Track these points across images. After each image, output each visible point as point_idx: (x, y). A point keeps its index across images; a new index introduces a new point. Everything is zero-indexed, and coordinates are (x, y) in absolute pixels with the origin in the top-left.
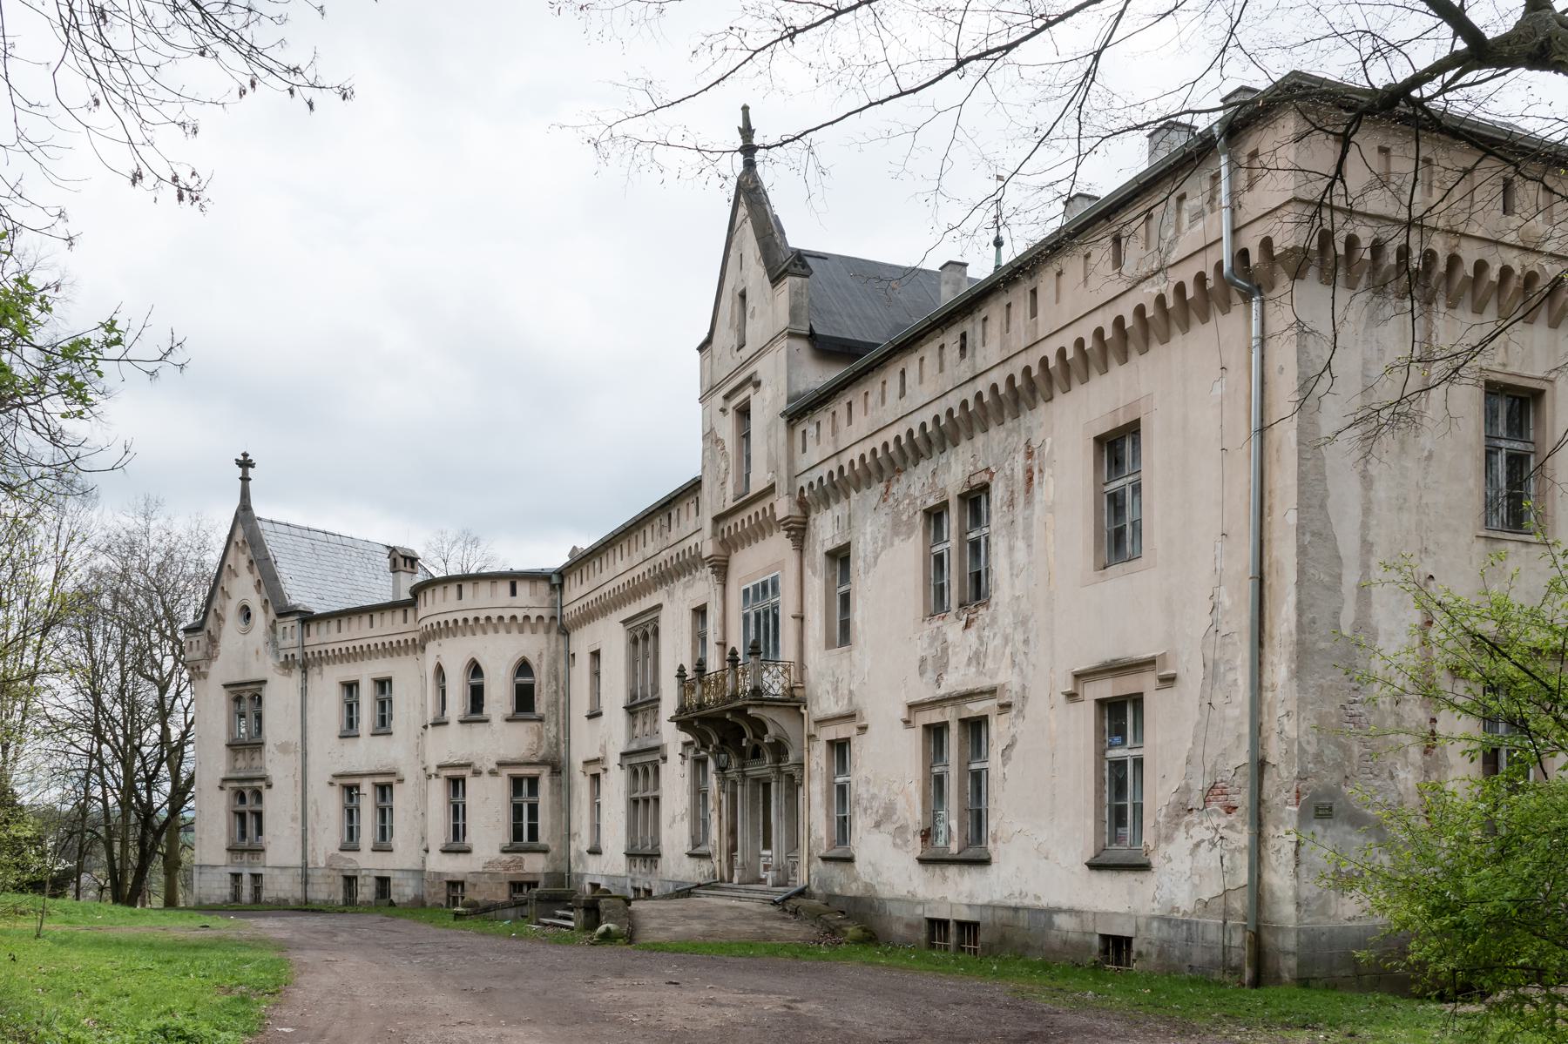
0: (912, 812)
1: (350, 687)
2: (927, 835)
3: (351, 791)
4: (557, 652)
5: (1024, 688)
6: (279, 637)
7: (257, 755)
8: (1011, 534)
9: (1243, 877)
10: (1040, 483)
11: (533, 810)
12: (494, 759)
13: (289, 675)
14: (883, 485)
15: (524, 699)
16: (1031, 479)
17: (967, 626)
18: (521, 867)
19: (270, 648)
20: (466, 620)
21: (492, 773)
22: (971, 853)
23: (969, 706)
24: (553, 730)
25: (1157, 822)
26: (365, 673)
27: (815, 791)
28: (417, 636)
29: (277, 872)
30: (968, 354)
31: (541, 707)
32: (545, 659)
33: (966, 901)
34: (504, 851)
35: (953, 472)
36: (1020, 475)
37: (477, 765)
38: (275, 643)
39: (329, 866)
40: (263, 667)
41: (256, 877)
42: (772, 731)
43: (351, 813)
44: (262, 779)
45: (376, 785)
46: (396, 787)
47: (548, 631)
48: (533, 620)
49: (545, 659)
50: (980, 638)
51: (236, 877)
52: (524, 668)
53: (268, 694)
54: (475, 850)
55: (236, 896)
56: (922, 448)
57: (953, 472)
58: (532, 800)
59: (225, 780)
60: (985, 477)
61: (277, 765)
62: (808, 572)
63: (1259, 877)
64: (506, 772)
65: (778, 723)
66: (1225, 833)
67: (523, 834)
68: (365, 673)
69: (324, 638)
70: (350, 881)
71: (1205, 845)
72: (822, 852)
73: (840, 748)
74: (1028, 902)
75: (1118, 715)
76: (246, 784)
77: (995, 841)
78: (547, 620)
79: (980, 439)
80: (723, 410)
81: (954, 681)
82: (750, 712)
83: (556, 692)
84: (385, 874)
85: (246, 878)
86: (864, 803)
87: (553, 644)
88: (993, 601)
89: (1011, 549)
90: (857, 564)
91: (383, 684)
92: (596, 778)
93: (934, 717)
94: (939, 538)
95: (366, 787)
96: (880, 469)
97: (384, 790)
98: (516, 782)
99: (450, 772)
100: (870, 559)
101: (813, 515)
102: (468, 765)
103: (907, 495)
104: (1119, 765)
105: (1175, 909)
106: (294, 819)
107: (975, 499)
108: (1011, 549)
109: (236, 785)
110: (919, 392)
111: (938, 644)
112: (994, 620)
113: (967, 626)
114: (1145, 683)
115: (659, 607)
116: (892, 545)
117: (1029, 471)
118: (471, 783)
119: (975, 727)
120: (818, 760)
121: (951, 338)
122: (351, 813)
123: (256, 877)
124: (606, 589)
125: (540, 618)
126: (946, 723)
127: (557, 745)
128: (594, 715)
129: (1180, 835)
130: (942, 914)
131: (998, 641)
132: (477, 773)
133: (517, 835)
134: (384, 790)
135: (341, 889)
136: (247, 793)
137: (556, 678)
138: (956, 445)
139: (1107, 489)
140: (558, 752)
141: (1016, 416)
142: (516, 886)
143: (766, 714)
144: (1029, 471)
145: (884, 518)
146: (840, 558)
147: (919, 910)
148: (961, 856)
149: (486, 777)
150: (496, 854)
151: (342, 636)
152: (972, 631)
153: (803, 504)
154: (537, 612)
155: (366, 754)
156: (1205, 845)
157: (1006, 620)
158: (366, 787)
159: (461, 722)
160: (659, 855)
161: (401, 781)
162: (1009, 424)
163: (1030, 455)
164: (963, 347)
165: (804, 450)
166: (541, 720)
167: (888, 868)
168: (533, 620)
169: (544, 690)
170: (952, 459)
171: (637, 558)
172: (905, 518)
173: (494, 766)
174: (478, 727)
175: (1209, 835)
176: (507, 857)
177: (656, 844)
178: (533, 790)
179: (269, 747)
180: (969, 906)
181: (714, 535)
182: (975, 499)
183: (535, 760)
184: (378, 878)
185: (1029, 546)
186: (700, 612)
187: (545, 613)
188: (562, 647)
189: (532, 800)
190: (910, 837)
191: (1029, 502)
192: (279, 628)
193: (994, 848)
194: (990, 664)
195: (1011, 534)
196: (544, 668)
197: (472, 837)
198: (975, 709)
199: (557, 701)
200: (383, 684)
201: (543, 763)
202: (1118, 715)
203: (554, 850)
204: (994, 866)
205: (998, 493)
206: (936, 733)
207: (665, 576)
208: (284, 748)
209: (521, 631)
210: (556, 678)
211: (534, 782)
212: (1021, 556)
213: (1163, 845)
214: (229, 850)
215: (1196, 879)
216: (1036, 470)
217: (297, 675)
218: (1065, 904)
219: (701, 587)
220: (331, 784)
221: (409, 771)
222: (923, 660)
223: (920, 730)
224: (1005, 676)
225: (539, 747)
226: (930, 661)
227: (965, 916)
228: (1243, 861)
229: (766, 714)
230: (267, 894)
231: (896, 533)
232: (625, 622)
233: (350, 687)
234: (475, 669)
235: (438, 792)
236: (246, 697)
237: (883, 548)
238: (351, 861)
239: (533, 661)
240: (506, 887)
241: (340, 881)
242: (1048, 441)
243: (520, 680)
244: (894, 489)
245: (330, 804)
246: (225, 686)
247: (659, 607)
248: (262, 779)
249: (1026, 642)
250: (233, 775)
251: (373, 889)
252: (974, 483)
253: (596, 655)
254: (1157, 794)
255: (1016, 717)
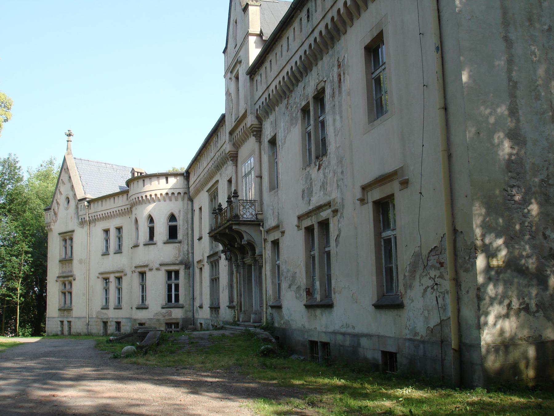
0: (302, 280)
1: (107, 231)
2: (309, 292)
3: (106, 280)
4: (188, 209)
5: (343, 199)
6: (79, 210)
7: (70, 265)
8: (334, 113)
9: (450, 312)
10: (344, 80)
11: (177, 286)
12: (159, 262)
13: (83, 228)
14: (286, 100)
15: (173, 232)
16: (340, 79)
17: (319, 169)
18: (171, 315)
19: (76, 216)
20: (156, 195)
21: (158, 269)
22: (325, 302)
23: (321, 214)
24: (186, 247)
25: (405, 276)
26: (112, 225)
27: (267, 270)
28: (129, 207)
29: (77, 320)
30: (310, 19)
31: (180, 236)
32: (182, 213)
33: (324, 330)
34: (163, 308)
35: (309, 86)
36: (336, 79)
37: (150, 266)
38: (78, 213)
39: (97, 317)
40: (72, 225)
41: (69, 322)
42: (246, 238)
43: (107, 291)
44: (72, 276)
45: (116, 278)
46: (124, 278)
47: (183, 200)
48: (176, 194)
49: (182, 213)
50: (324, 174)
51: (62, 322)
52: (172, 218)
53: (75, 237)
54: (150, 307)
55: (62, 331)
56: (298, 76)
57: (309, 86)
58: (176, 282)
59: (58, 277)
60: (323, 84)
61: (77, 269)
62: (263, 153)
63: (459, 311)
64: (164, 268)
65: (249, 233)
66: (438, 280)
67: (172, 297)
68: (112, 225)
69: (100, 209)
70: (105, 323)
71: (429, 289)
72: (270, 303)
73: (276, 244)
74: (350, 330)
75: (383, 209)
76: (66, 279)
77: (335, 293)
78: (182, 194)
79: (320, 63)
80: (230, 79)
81: (317, 200)
82: (234, 227)
83: (187, 229)
84: (119, 320)
85: (66, 323)
86: (285, 274)
87: (186, 206)
88: (328, 152)
89: (334, 120)
90: (279, 142)
91: (119, 229)
92: (201, 269)
93: (307, 223)
94: (309, 124)
95: (112, 278)
96: (284, 93)
97: (119, 279)
98: (169, 273)
99: (140, 270)
100: (283, 141)
101: (264, 123)
102: (147, 266)
103: (295, 103)
104: (388, 241)
105: (416, 334)
106: (84, 295)
107: (319, 97)
108: (334, 120)
109: (62, 279)
110: (294, 46)
111: (308, 181)
112: (329, 162)
113: (319, 169)
114: (394, 187)
115: (217, 181)
116: (290, 131)
117: (339, 75)
118: (149, 275)
119: (325, 225)
120: (268, 253)
121: (303, 14)
122: (107, 291)
123: (69, 322)
124: (202, 176)
125: (179, 193)
126: (313, 225)
127: (188, 254)
128: (200, 239)
129: (416, 283)
130: (315, 339)
131: (331, 175)
132: (151, 270)
133: (170, 300)
134: (119, 279)
135: (102, 328)
136: (67, 283)
137: (187, 222)
138: (311, 70)
139: (374, 76)
140: (188, 258)
141: (333, 47)
142: (169, 325)
143: (242, 229)
144: (339, 75)
145: (287, 118)
146: (273, 142)
147: (306, 336)
148: (321, 303)
149: (154, 271)
150: (159, 309)
151: (104, 208)
152: (321, 171)
153: (258, 117)
154: (178, 191)
155: (113, 263)
156: (429, 289)
157: (334, 162)
158: (112, 278)
159: (145, 245)
160: (219, 308)
161: (126, 275)
162: (331, 52)
163: (339, 66)
164: (308, 17)
165: (257, 90)
166: (180, 242)
167: (294, 313)
168: (176, 194)
169: (181, 227)
170: (310, 79)
171: (209, 159)
172: (294, 115)
173: (158, 266)
174: (152, 247)
175: (431, 283)
176: (164, 311)
177: (219, 304)
178: (177, 277)
179: (75, 262)
180: (325, 333)
181: (230, 141)
182: (319, 97)
183: (177, 262)
184: (116, 322)
185: (341, 117)
186: (230, 181)
187: (181, 191)
188: (190, 207)
189: (176, 282)
190: (302, 292)
191: (340, 93)
192: (79, 206)
193: (337, 298)
194: (329, 189)
195: (334, 113)
196: (181, 217)
197: (149, 301)
198: (324, 215)
199: (188, 234)
200: (119, 229)
201: (181, 263)
202: (383, 209)
203: (187, 306)
204: (335, 308)
205: (328, 92)
206: (309, 230)
207: (218, 167)
208: (81, 261)
209: (171, 200)
210: (187, 222)
211: (177, 273)
212: (338, 124)
213: (409, 291)
214: (59, 310)
215: (426, 313)
216: (342, 74)
217: (86, 228)
218: (365, 331)
219: (228, 170)
220: (98, 277)
221: (128, 271)
222: (303, 191)
223: (303, 230)
224: (335, 195)
225: (179, 255)
226: (306, 191)
227: (325, 339)
228: (449, 300)
229: (242, 229)
230: (73, 330)
231: (292, 124)
232: (207, 191)
233: (107, 231)
234: (151, 219)
235: (136, 280)
236: (67, 237)
237: (288, 133)
238: (106, 314)
239: (177, 215)
240: (164, 325)
241: (102, 324)
242: (346, 56)
243: (171, 224)
244: (290, 102)
245: (99, 285)
246: (59, 234)
247: (217, 181)
248: (72, 276)
249: (342, 172)
250: (62, 275)
251: (114, 327)
252: (319, 88)
253: (200, 209)
254: (404, 258)
255: (340, 217)
